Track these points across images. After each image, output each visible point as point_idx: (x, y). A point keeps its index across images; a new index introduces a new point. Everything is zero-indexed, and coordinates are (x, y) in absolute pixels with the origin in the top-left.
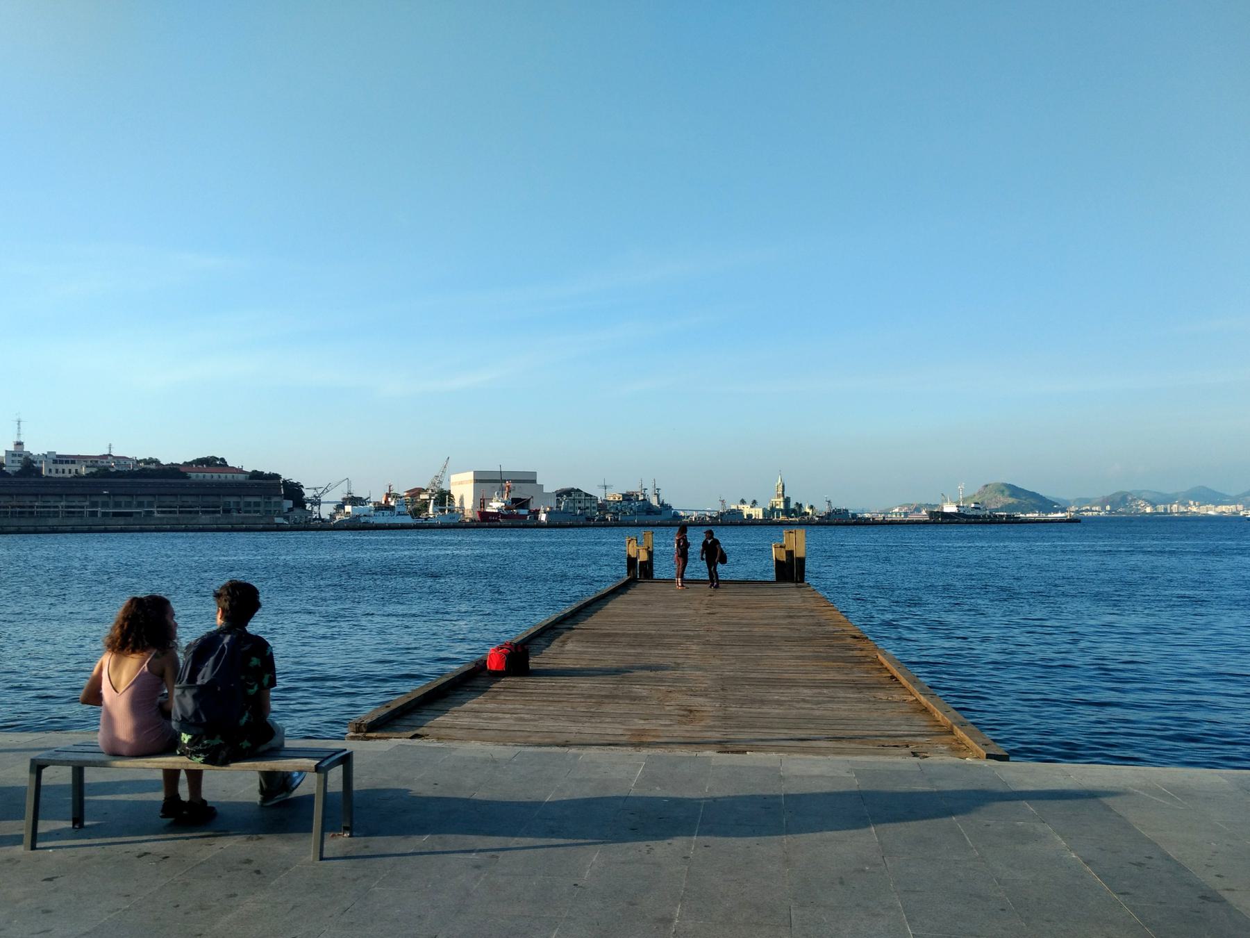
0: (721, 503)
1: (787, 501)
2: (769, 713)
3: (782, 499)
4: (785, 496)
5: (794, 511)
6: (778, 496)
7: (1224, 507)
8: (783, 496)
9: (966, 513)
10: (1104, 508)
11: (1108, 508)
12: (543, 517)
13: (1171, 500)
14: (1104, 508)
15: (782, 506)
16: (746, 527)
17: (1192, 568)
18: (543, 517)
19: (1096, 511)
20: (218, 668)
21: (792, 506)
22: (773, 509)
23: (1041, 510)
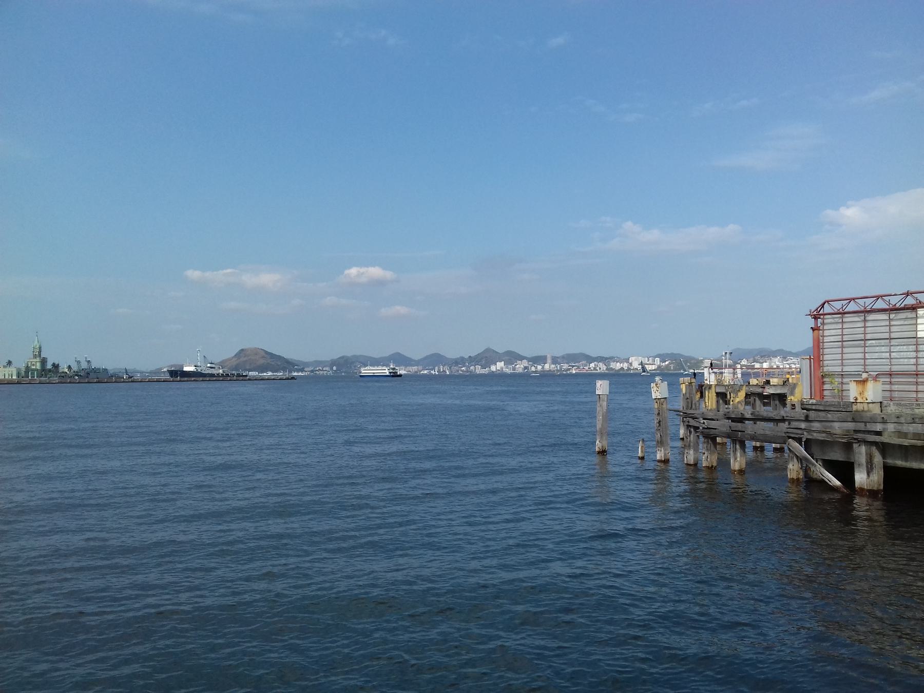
0: (86, 363)
1: (44, 362)
2: (149, 527)
3: (38, 359)
4: (42, 356)
5: (50, 370)
6: (35, 356)
7: (410, 367)
8: (40, 355)
9: (203, 372)
10: (332, 369)
11: (335, 368)
12: (672, 368)
13: (767, 354)
14: (332, 369)
15: (38, 366)
16: (720, 387)
17: (480, 417)
18: (672, 368)
19: (327, 371)
20: (151, 664)
21: (49, 366)
22: (28, 369)
23: (284, 369)
